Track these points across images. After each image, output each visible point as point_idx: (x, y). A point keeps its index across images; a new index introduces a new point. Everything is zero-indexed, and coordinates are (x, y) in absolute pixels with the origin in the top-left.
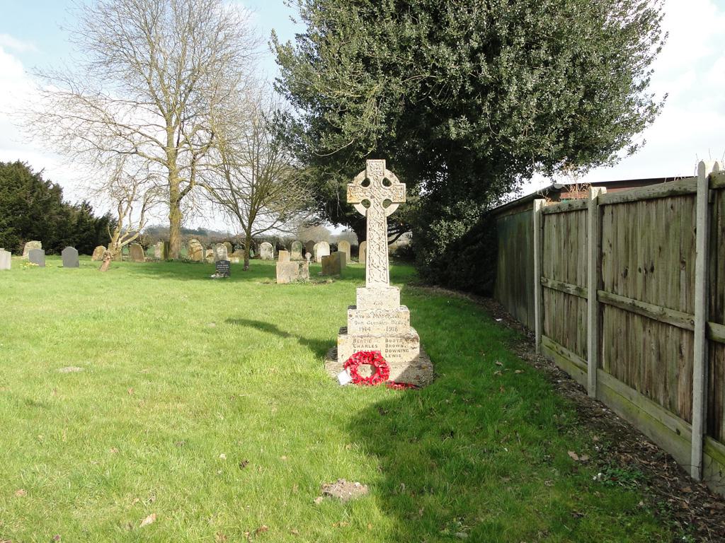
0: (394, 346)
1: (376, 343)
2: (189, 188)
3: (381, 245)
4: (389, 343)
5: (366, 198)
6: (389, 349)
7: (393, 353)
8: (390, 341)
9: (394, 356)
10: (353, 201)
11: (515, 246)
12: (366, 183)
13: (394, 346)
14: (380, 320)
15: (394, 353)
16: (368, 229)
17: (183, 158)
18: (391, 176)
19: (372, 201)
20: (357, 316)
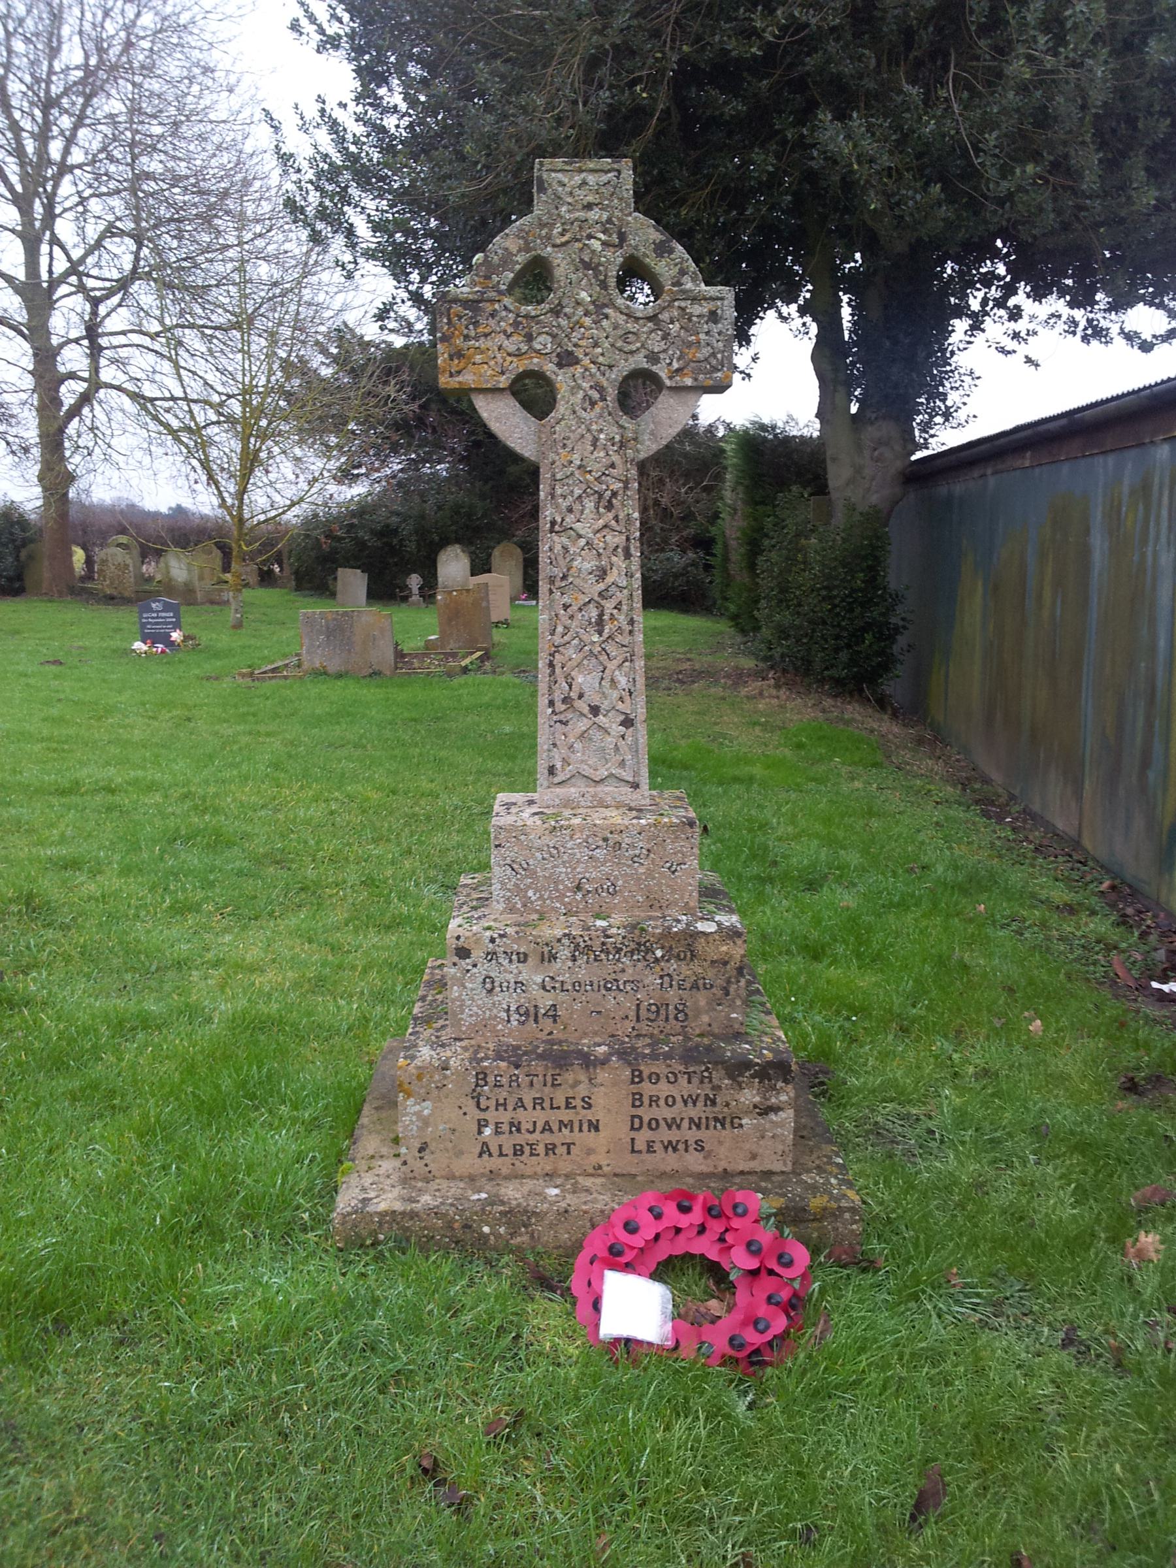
0: (670, 1101)
1: (582, 1090)
2: (85, 399)
3: (609, 605)
4: (647, 1088)
5: (535, 363)
6: (646, 1114)
7: (665, 1134)
8: (655, 1078)
9: (671, 1146)
10: (468, 378)
11: (1058, 613)
12: (536, 278)
13: (670, 1101)
14: (606, 969)
15: (673, 1135)
16: (945, 448)
17: (68, 316)
18: (662, 250)
19: (562, 379)
20: (491, 956)
